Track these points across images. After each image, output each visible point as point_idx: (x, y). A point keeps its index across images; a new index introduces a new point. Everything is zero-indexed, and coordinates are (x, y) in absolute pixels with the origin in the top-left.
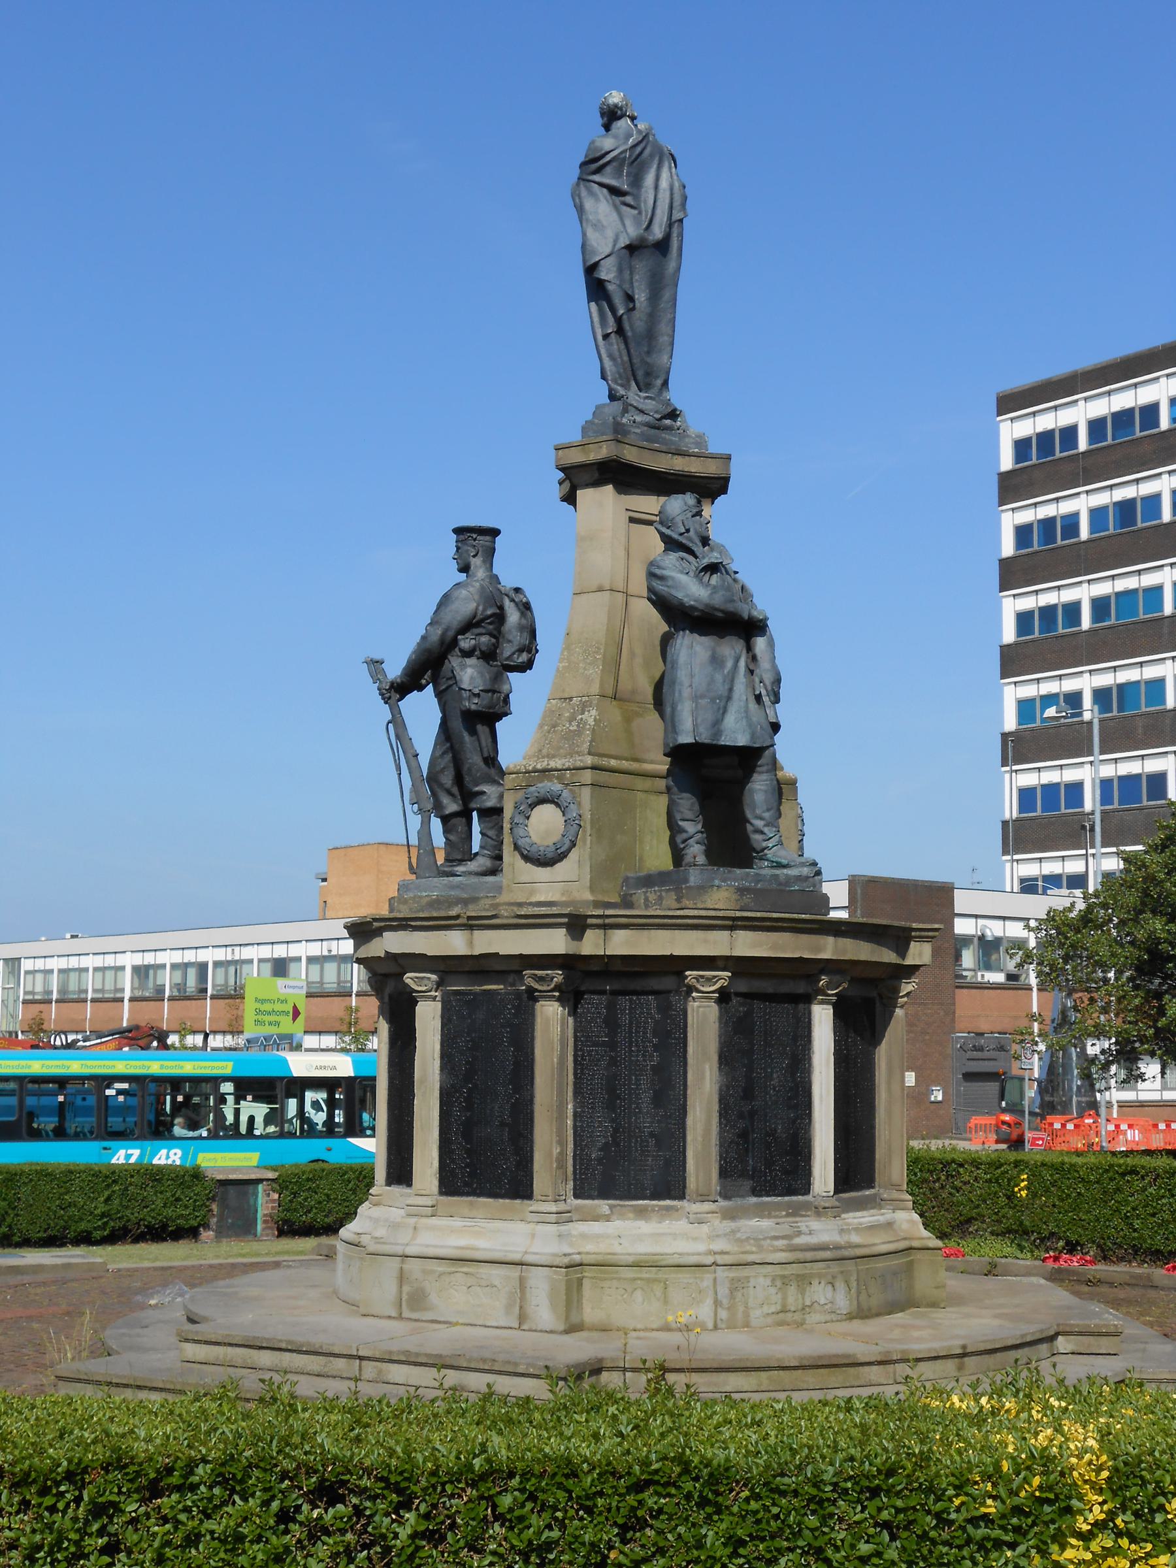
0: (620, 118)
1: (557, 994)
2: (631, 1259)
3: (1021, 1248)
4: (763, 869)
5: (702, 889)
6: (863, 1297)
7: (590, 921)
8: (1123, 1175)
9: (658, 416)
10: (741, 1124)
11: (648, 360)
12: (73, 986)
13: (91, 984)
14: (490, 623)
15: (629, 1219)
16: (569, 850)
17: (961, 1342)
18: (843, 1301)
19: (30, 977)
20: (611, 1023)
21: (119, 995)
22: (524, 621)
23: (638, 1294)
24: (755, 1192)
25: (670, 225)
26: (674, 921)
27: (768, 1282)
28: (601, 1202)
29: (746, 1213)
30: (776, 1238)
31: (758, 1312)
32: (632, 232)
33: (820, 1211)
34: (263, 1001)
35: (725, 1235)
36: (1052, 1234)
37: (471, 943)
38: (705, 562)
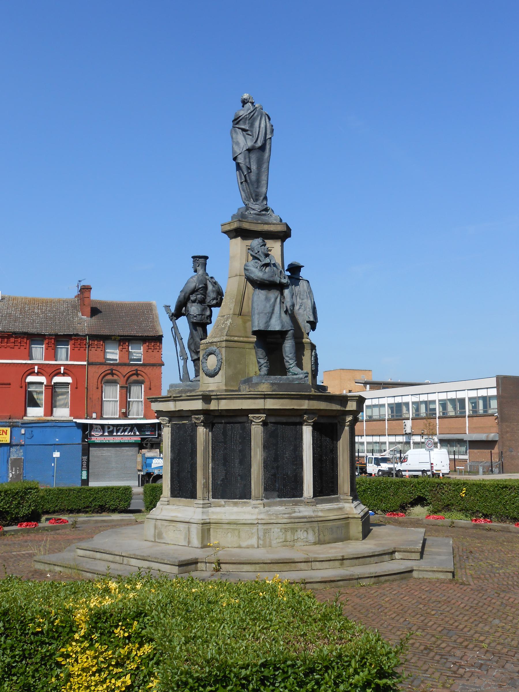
0: (247, 103)
2: (227, 521)
3: (466, 516)
4: (290, 376)
5: (257, 384)
6: (321, 536)
7: (212, 397)
8: (502, 488)
9: (259, 211)
10: (273, 471)
11: (257, 190)
16: (218, 371)
17: (341, 555)
18: (311, 537)
20: (225, 434)
22: (214, 289)
23: (229, 534)
24: (279, 497)
25: (265, 140)
30: (285, 514)
31: (275, 542)
32: (250, 144)
33: (308, 503)
36: (477, 511)
37: (175, 406)
38: (263, 263)
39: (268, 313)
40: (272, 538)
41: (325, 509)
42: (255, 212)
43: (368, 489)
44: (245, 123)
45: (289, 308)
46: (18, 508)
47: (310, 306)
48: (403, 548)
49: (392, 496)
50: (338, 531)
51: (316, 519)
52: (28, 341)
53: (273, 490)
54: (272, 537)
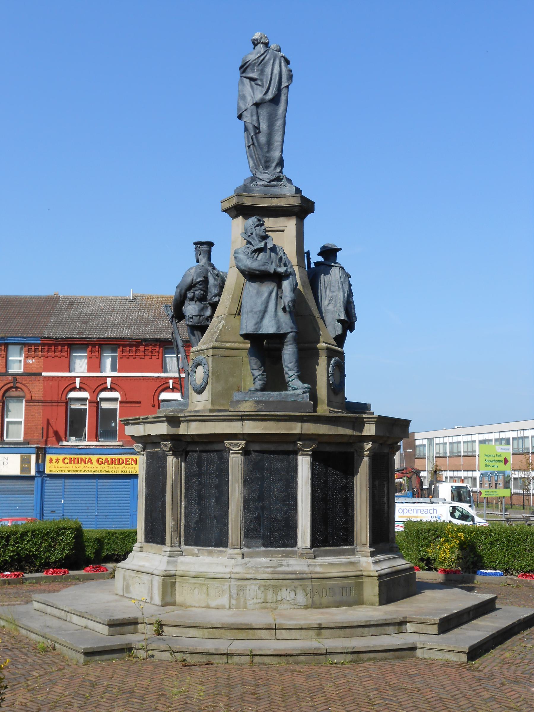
1: (171, 452)
2: (194, 574)
6: (316, 598)
9: (268, 181)
10: (256, 513)
11: (267, 155)
12: (455, 450)
13: (462, 449)
14: (200, 285)
15: (205, 556)
16: (205, 386)
19: (438, 446)
21: (474, 454)
22: (216, 283)
23: (196, 591)
24: (264, 545)
26: (221, 418)
27: (257, 588)
28: (195, 547)
29: (258, 555)
30: (268, 567)
31: (251, 602)
32: (259, 96)
34: (489, 456)
35: (241, 565)
39: (260, 311)
40: (247, 598)
41: (330, 564)
42: (263, 183)
43: (497, 541)
44: (253, 71)
45: (287, 304)
46: (49, 551)
47: (342, 300)
48: (415, 618)
49: (529, 551)
50: (349, 591)
51: (309, 576)
52: (161, 349)
53: (256, 537)
54: (247, 596)
